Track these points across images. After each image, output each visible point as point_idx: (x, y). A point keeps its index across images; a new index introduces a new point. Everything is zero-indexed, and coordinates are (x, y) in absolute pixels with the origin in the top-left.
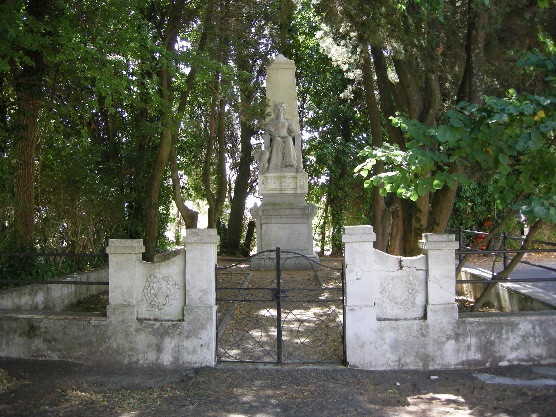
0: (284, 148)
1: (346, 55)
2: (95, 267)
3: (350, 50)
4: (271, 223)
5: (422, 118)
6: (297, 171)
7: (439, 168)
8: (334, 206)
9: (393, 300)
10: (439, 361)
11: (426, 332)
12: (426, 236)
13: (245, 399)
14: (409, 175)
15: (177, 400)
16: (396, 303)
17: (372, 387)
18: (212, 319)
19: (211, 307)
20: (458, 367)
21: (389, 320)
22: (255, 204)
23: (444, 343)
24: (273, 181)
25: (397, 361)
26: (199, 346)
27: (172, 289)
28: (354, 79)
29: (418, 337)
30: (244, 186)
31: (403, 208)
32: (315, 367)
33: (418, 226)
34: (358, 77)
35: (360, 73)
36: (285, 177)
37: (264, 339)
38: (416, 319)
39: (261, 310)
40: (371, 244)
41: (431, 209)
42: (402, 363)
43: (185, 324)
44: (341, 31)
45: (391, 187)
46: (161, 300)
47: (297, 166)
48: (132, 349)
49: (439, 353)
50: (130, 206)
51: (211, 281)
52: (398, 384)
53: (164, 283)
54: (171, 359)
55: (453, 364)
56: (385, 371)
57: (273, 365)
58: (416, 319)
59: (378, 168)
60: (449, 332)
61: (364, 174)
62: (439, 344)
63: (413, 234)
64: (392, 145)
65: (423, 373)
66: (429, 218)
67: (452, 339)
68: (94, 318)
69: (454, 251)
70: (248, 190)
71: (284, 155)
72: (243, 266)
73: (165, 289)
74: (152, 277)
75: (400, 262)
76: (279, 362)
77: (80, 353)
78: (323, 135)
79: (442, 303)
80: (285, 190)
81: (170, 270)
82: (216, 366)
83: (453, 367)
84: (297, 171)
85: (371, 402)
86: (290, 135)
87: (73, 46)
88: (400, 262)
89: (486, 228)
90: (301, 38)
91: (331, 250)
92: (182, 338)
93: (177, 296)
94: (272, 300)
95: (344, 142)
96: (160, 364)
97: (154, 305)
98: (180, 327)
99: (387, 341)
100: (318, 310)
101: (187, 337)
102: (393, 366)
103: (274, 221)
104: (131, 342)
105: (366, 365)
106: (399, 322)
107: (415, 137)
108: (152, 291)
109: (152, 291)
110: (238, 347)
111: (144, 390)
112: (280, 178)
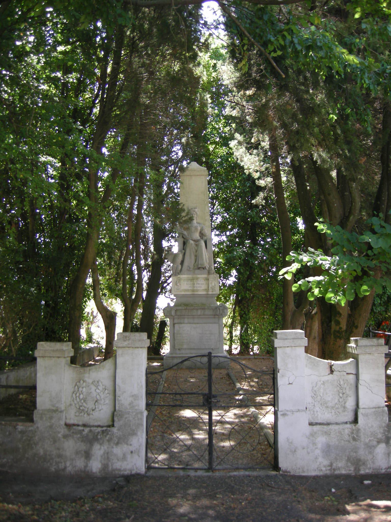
0: (196, 251)
1: (257, 164)
2: (15, 365)
3: (261, 159)
4: (184, 323)
5: (343, 223)
6: (209, 273)
7: (365, 273)
8: (242, 307)
9: (324, 404)
10: (370, 464)
11: (357, 436)
12: (356, 341)
13: (182, 510)
14: (337, 280)
15: (111, 512)
16: (327, 407)
17: (308, 494)
18: (142, 425)
19: (142, 413)
20: (388, 470)
21: (320, 424)
22: (169, 304)
23: (375, 447)
24: (186, 283)
25: (329, 466)
26: (129, 452)
27: (101, 394)
28: (265, 186)
29: (349, 441)
30: (156, 286)
31: (321, 311)
32: (247, 473)
33: (337, 328)
34: (270, 185)
35: (270, 181)
36: (197, 279)
37: (190, 442)
38: (346, 423)
39: (180, 410)
40: (303, 349)
41: (350, 312)
42: (333, 467)
43: (115, 430)
44: (253, 141)
45: (320, 291)
46: (90, 405)
47: (209, 268)
48: (60, 456)
49: (370, 457)
50: (47, 305)
51: (142, 386)
52: (333, 490)
53: (93, 388)
54: (99, 466)
55: (384, 468)
56: (317, 476)
57: (204, 471)
58: (346, 423)
59: (304, 272)
60: (380, 436)
61: (289, 277)
62: (370, 448)
63: (332, 336)
64: (316, 250)
65: (355, 477)
66: (348, 321)
67: (383, 442)
68: (20, 424)
69: (384, 355)
70: (159, 291)
71: (197, 257)
72: (155, 364)
73: (94, 394)
74: (82, 382)
75: (331, 367)
76: (210, 468)
77: (5, 460)
78: (231, 238)
79: (371, 406)
80: (197, 291)
81: (101, 374)
82: (146, 472)
83: (383, 471)
84: (209, 273)
85: (311, 511)
86: (202, 238)
87: (6, 147)
88: (331, 367)
89: (385, 327)
90: (211, 148)
91: (239, 349)
92: (112, 444)
93: (107, 401)
94: (204, 405)
95: (252, 246)
96: (88, 472)
97: (83, 410)
98: (110, 433)
99: (319, 446)
100: (237, 411)
101: (117, 444)
102: (325, 471)
103: (186, 320)
104: (58, 449)
105: (298, 471)
106: (330, 427)
107: (340, 243)
108: (81, 396)
109: (81, 396)
110: (164, 451)
111: (74, 501)
112: (192, 279)
